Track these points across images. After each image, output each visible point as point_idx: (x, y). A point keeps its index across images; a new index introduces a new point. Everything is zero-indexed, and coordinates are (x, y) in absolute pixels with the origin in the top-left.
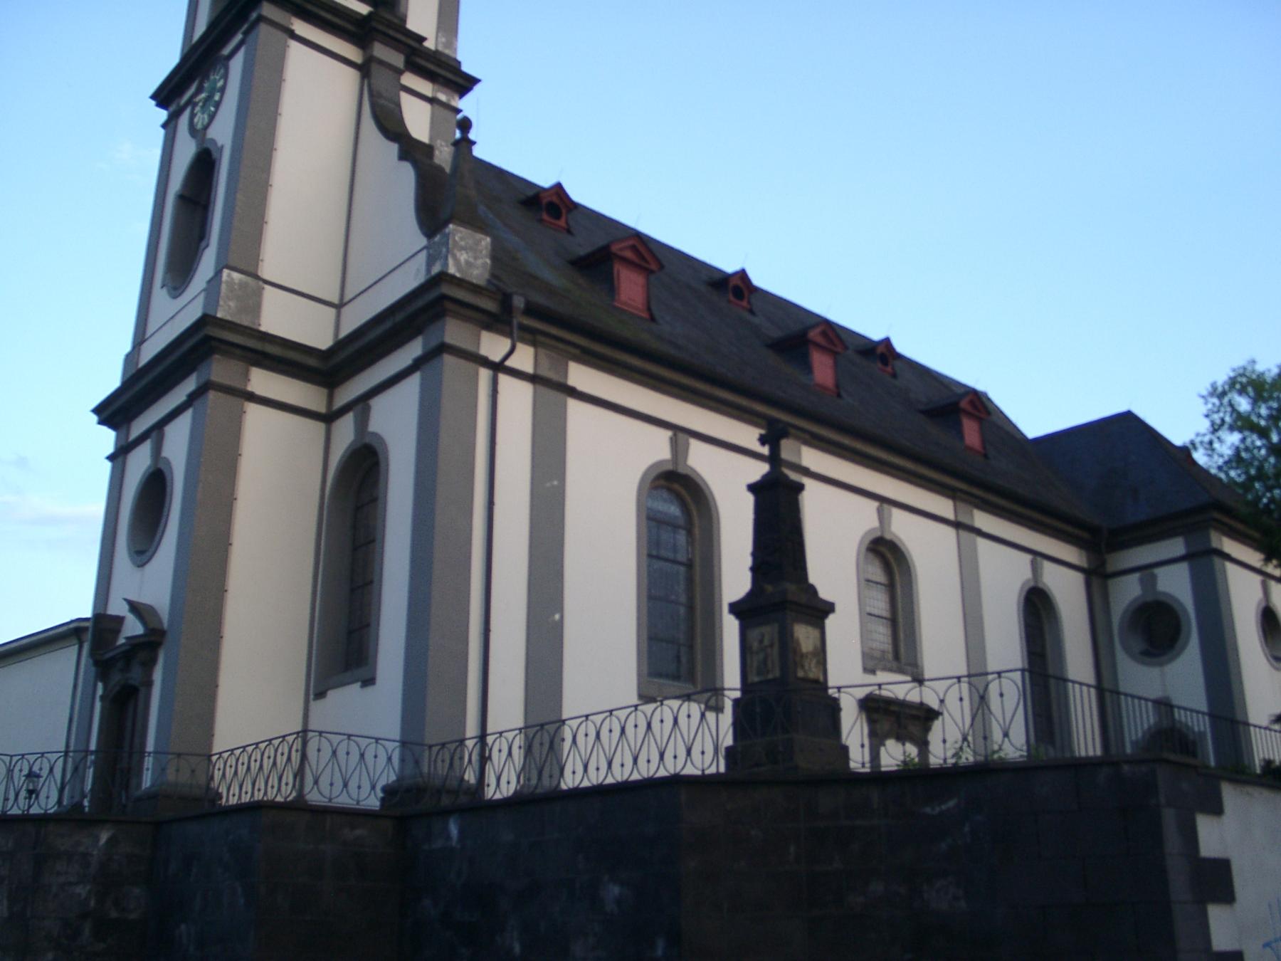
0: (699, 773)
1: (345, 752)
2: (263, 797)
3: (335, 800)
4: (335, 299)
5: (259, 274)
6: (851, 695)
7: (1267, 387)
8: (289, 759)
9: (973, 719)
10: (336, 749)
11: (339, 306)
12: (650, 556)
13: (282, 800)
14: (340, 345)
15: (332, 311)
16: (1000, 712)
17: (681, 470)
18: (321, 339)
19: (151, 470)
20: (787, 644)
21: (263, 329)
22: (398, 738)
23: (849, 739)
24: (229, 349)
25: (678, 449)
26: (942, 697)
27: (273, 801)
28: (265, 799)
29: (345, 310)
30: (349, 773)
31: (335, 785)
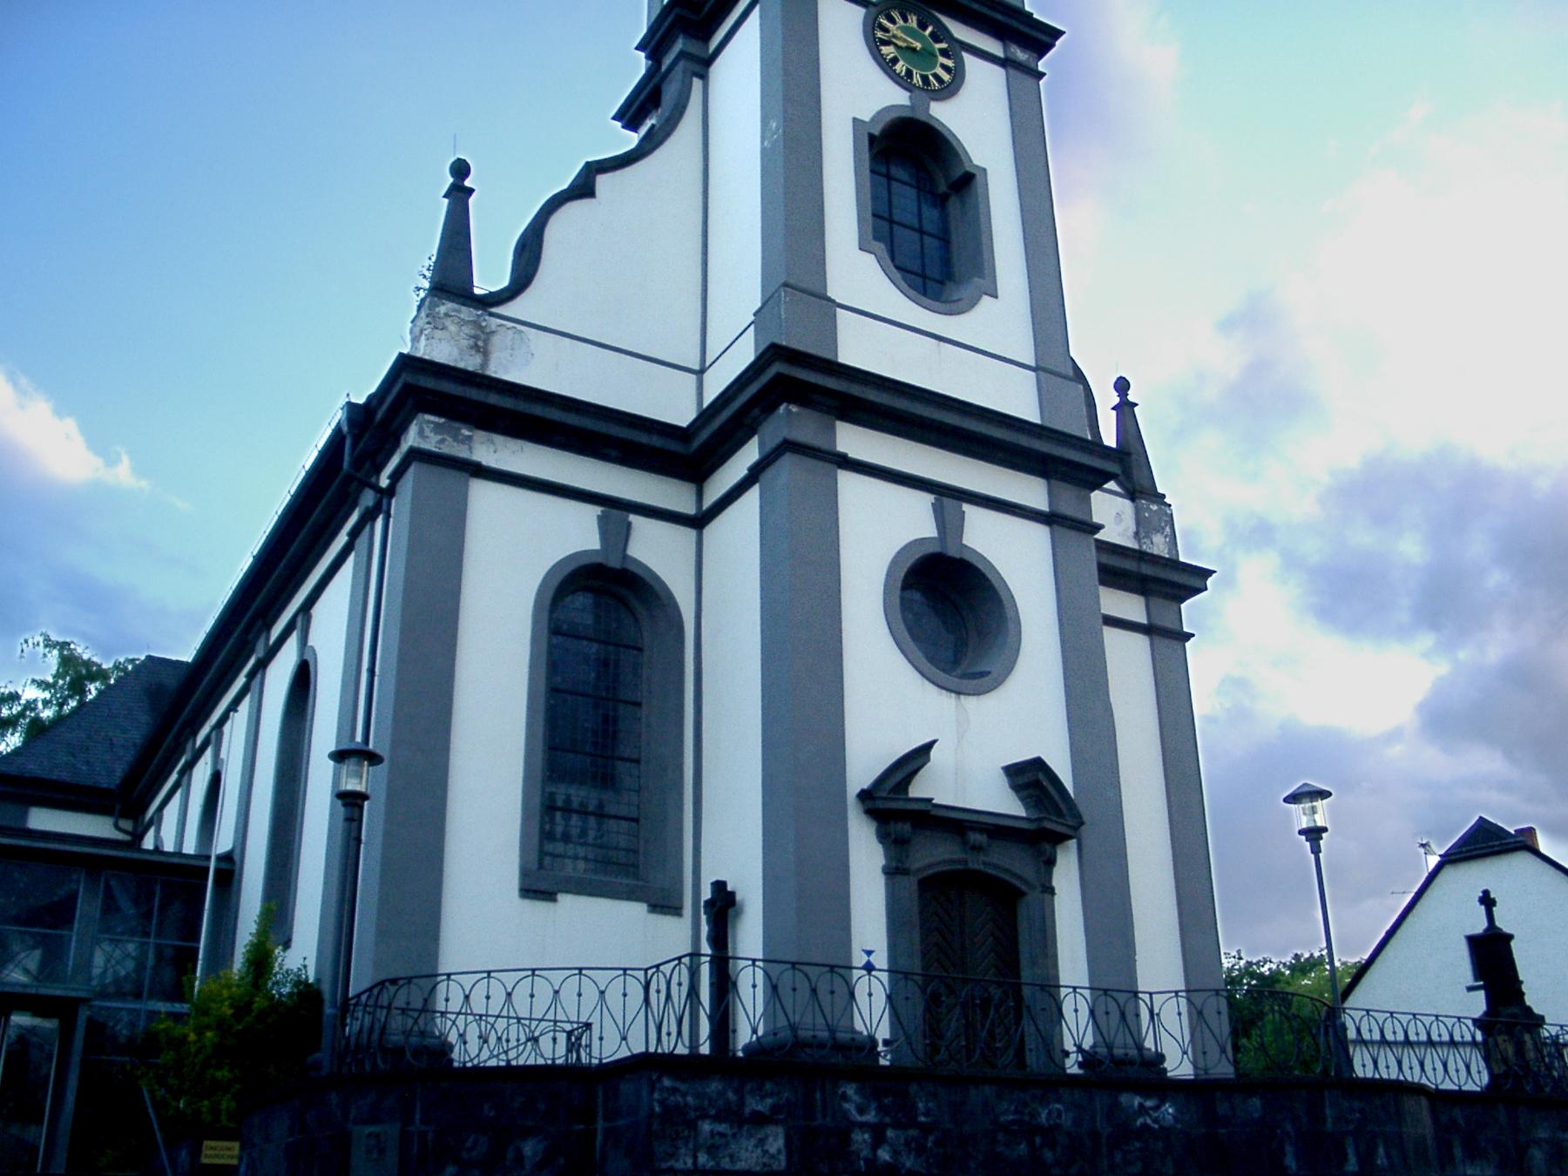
0: (1457, 1088)
1: (451, 1000)
2: (656, 1049)
3: (1211, 1071)
4: (697, 367)
5: (829, 294)
6: (634, 977)
7: (58, 647)
8: (668, 997)
9: (1192, 1035)
10: (816, 987)
11: (701, 372)
12: (550, 748)
13: (686, 1051)
14: (705, 416)
15: (694, 377)
16: (622, 1022)
17: (953, 552)
18: (682, 414)
19: (298, 663)
20: (899, 861)
21: (841, 360)
22: (886, 967)
23: (632, 1050)
24: (805, 396)
25: (948, 523)
26: (557, 988)
27: (671, 1055)
28: (659, 1051)
29: (706, 376)
30: (874, 1026)
31: (558, 1041)
